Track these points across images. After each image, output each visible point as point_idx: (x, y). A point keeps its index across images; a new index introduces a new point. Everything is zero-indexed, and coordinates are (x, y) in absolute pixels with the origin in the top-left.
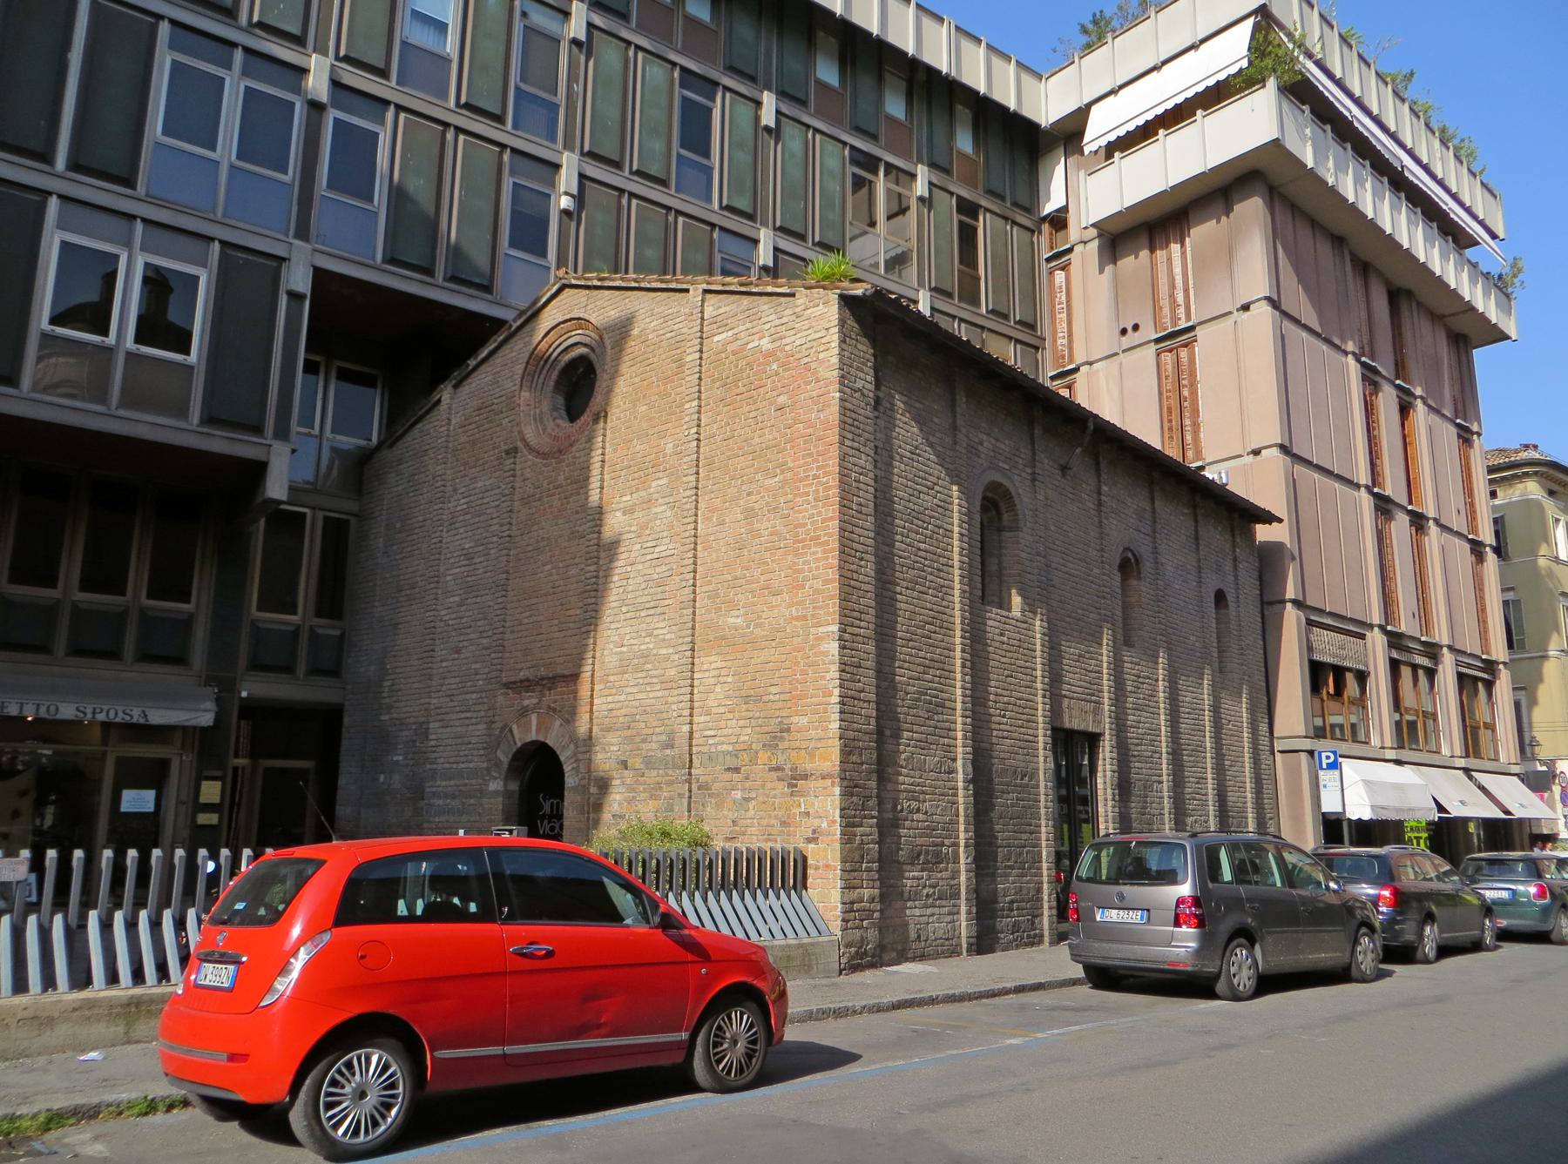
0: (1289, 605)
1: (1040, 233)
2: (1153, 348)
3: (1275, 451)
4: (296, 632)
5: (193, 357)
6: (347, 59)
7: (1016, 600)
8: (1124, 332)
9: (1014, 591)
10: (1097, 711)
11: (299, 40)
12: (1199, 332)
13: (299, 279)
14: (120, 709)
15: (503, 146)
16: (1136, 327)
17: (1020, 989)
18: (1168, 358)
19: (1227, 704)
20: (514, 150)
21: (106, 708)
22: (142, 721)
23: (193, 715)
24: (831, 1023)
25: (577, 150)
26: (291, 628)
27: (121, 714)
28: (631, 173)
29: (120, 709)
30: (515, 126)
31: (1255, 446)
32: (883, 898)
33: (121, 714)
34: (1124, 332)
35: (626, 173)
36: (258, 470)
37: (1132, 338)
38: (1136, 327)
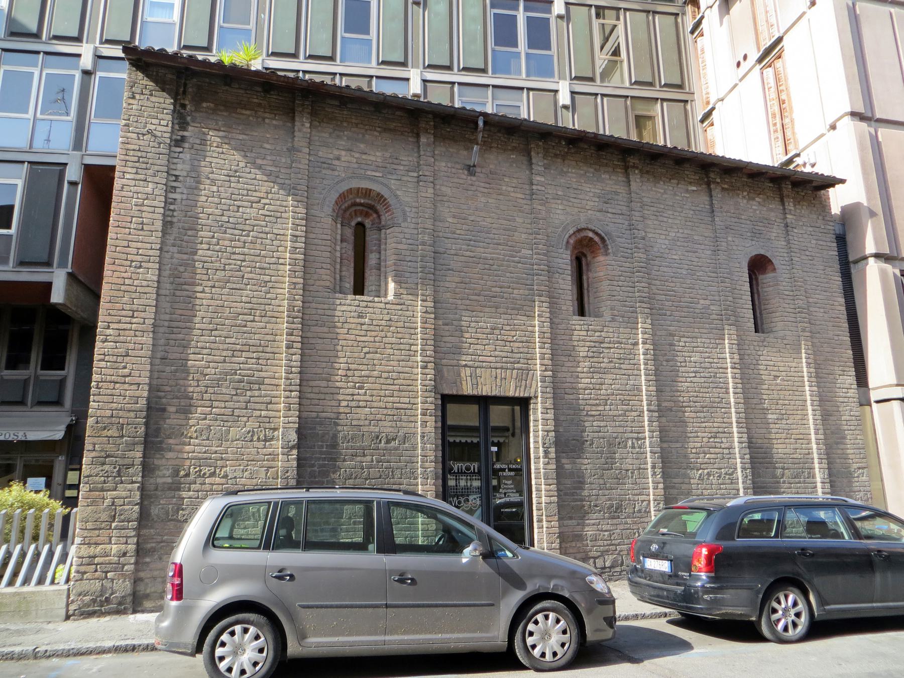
0: (871, 260)
1: (684, 14)
2: (758, 67)
3: (847, 119)
4: (26, 382)
5: (13, 231)
6: (576, 78)
7: (391, 286)
8: (739, 64)
9: (390, 279)
10: (525, 373)
11: (404, 64)
12: (785, 42)
13: (73, 173)
14: (12, 433)
15: (453, 83)
16: (745, 57)
17: (117, 650)
18: (769, 72)
19: (691, 356)
20: (460, 84)
21: (4, 432)
22: (23, 439)
23: (52, 433)
24: (648, 613)
25: (568, 78)
26: (60, 378)
27: (12, 436)
28: (661, 86)
29: (12, 433)
30: (528, 75)
31: (830, 121)
32: (140, 552)
33: (12, 436)
34: (739, 64)
35: (658, 88)
36: (48, 286)
37: (745, 66)
38: (745, 57)
